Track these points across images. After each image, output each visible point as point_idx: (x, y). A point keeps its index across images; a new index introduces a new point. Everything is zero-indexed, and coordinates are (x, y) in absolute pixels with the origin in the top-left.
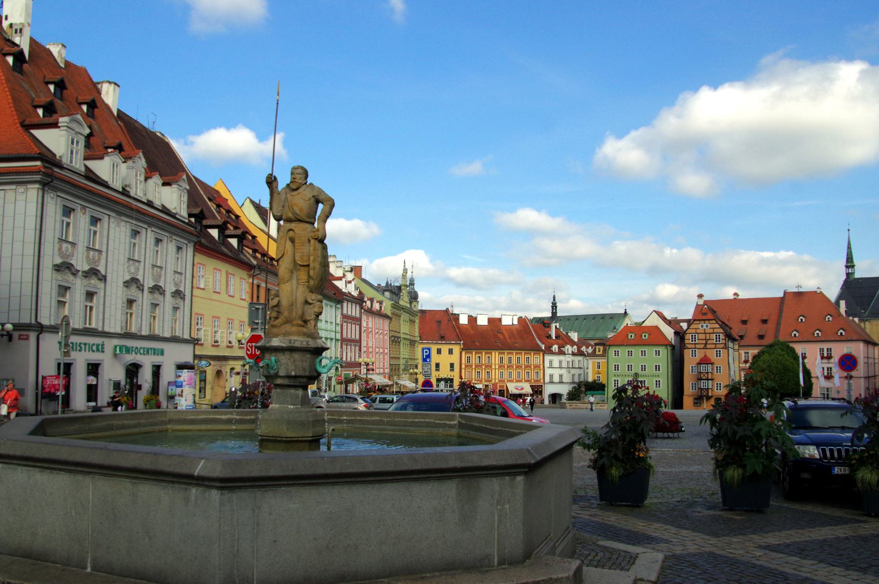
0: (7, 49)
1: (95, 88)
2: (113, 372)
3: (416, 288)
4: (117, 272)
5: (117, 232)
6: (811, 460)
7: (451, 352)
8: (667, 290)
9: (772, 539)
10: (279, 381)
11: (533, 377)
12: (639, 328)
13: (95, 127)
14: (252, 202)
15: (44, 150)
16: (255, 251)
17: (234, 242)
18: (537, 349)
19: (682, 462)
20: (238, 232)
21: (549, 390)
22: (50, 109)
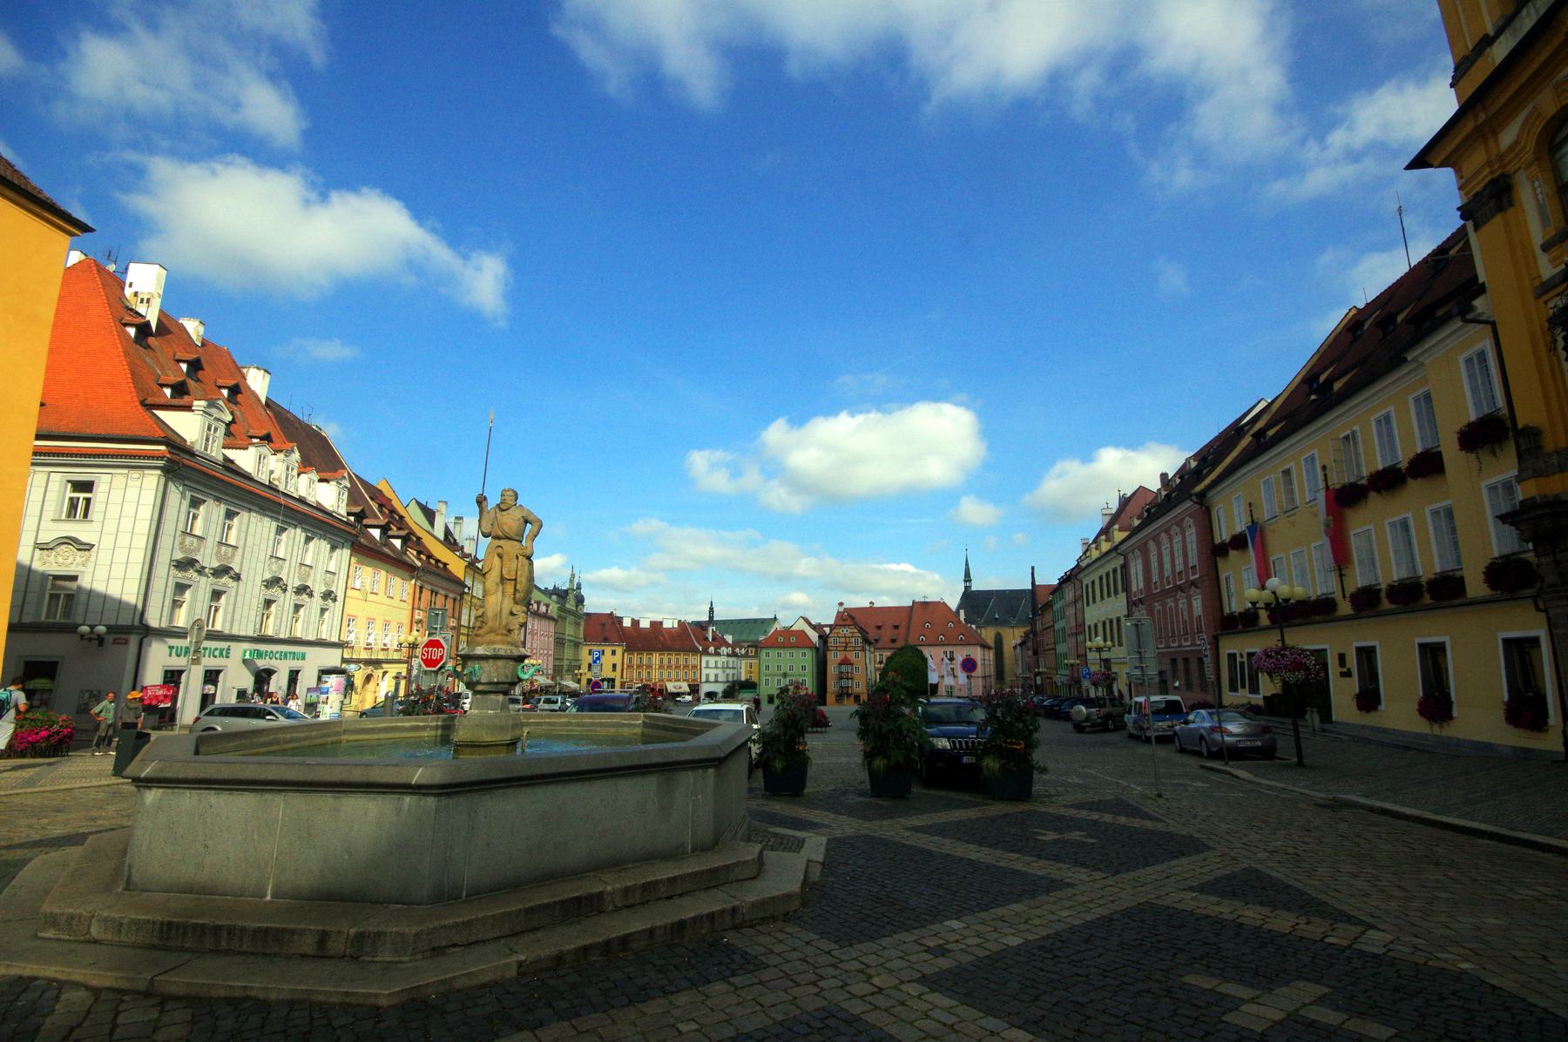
0: (128, 319)
1: (238, 371)
2: (236, 680)
3: (583, 592)
4: (255, 571)
5: (254, 530)
6: (943, 751)
7: (614, 653)
8: (798, 598)
9: (917, 821)
10: (480, 688)
11: (691, 675)
12: (787, 632)
13: (238, 413)
14: (419, 503)
15: (170, 434)
16: (419, 553)
17: (397, 543)
18: (695, 651)
19: (835, 751)
20: (403, 533)
21: (705, 688)
22: (180, 389)
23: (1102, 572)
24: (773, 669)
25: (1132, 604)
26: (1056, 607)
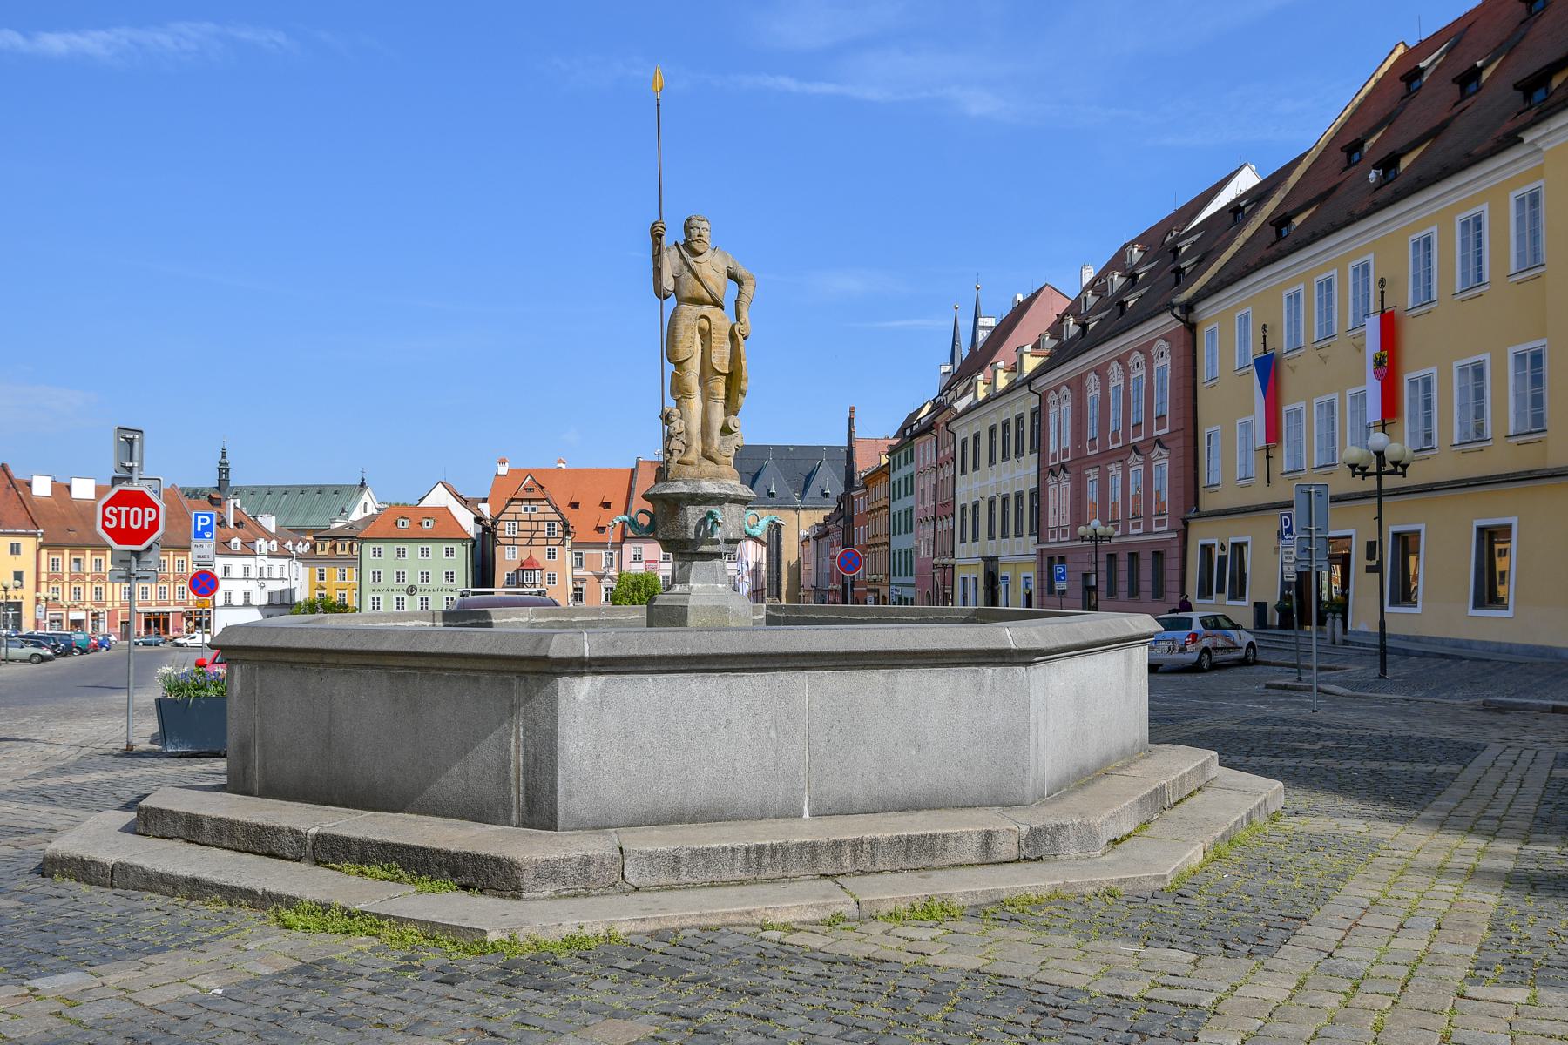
23: (996, 419)
24: (389, 579)
25: (1046, 471)
26: (894, 477)
